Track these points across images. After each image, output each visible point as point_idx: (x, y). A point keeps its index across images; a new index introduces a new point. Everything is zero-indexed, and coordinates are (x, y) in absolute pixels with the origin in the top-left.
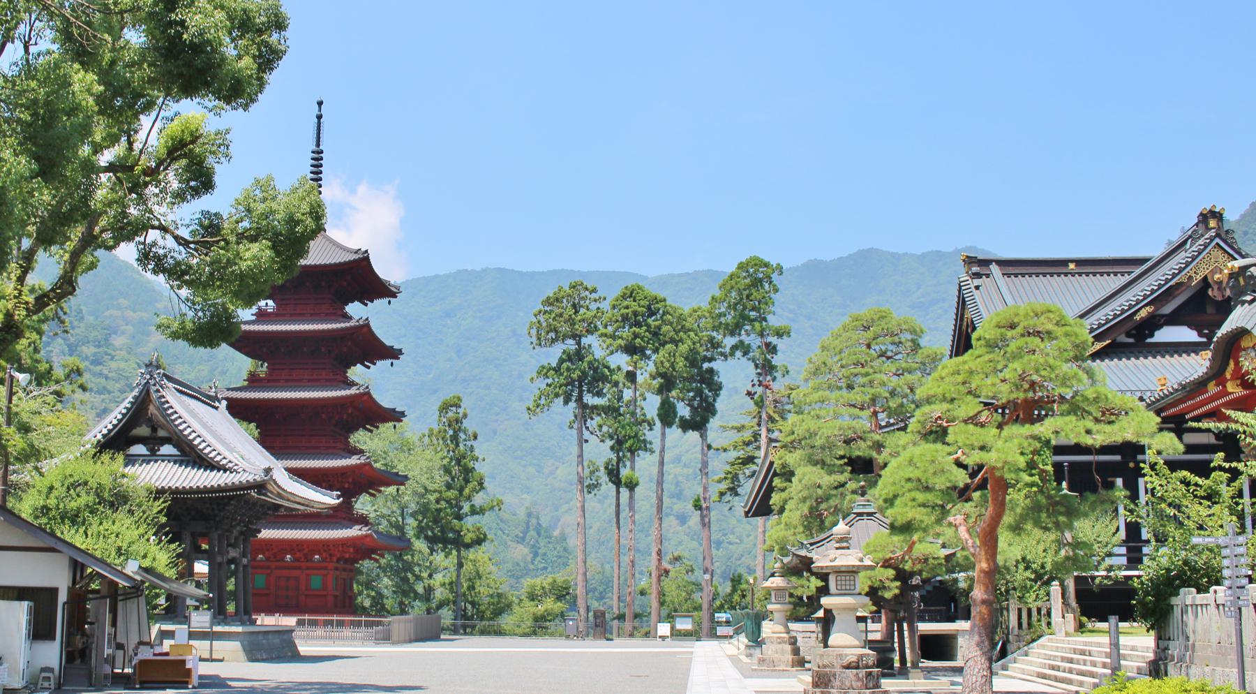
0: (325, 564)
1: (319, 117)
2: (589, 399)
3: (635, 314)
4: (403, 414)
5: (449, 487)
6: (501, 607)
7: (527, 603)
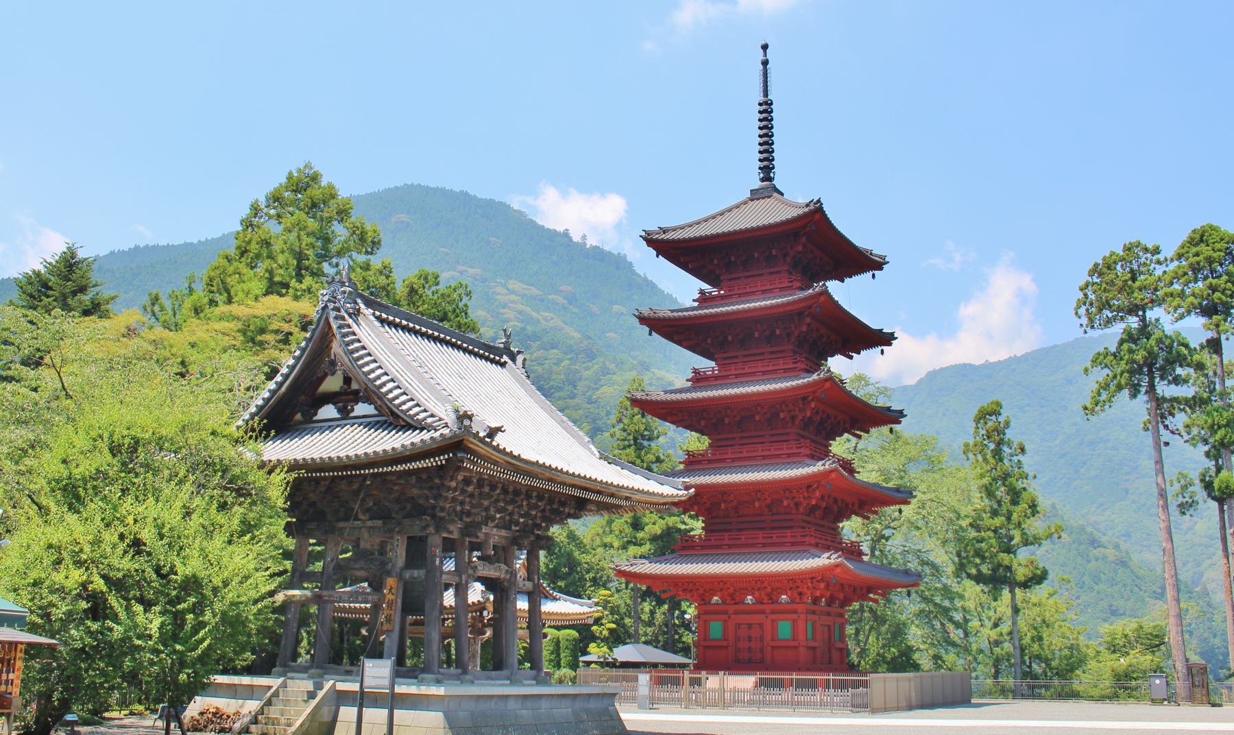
0: (795, 606)
1: (765, 63)
2: (1165, 389)
3: (1210, 261)
4: (901, 414)
5: (994, 513)
6: (1073, 663)
7: (1106, 655)
